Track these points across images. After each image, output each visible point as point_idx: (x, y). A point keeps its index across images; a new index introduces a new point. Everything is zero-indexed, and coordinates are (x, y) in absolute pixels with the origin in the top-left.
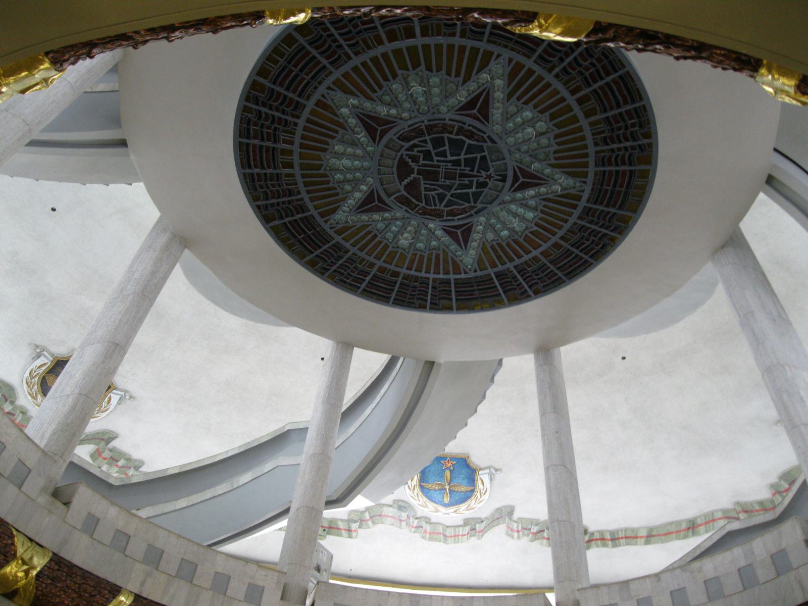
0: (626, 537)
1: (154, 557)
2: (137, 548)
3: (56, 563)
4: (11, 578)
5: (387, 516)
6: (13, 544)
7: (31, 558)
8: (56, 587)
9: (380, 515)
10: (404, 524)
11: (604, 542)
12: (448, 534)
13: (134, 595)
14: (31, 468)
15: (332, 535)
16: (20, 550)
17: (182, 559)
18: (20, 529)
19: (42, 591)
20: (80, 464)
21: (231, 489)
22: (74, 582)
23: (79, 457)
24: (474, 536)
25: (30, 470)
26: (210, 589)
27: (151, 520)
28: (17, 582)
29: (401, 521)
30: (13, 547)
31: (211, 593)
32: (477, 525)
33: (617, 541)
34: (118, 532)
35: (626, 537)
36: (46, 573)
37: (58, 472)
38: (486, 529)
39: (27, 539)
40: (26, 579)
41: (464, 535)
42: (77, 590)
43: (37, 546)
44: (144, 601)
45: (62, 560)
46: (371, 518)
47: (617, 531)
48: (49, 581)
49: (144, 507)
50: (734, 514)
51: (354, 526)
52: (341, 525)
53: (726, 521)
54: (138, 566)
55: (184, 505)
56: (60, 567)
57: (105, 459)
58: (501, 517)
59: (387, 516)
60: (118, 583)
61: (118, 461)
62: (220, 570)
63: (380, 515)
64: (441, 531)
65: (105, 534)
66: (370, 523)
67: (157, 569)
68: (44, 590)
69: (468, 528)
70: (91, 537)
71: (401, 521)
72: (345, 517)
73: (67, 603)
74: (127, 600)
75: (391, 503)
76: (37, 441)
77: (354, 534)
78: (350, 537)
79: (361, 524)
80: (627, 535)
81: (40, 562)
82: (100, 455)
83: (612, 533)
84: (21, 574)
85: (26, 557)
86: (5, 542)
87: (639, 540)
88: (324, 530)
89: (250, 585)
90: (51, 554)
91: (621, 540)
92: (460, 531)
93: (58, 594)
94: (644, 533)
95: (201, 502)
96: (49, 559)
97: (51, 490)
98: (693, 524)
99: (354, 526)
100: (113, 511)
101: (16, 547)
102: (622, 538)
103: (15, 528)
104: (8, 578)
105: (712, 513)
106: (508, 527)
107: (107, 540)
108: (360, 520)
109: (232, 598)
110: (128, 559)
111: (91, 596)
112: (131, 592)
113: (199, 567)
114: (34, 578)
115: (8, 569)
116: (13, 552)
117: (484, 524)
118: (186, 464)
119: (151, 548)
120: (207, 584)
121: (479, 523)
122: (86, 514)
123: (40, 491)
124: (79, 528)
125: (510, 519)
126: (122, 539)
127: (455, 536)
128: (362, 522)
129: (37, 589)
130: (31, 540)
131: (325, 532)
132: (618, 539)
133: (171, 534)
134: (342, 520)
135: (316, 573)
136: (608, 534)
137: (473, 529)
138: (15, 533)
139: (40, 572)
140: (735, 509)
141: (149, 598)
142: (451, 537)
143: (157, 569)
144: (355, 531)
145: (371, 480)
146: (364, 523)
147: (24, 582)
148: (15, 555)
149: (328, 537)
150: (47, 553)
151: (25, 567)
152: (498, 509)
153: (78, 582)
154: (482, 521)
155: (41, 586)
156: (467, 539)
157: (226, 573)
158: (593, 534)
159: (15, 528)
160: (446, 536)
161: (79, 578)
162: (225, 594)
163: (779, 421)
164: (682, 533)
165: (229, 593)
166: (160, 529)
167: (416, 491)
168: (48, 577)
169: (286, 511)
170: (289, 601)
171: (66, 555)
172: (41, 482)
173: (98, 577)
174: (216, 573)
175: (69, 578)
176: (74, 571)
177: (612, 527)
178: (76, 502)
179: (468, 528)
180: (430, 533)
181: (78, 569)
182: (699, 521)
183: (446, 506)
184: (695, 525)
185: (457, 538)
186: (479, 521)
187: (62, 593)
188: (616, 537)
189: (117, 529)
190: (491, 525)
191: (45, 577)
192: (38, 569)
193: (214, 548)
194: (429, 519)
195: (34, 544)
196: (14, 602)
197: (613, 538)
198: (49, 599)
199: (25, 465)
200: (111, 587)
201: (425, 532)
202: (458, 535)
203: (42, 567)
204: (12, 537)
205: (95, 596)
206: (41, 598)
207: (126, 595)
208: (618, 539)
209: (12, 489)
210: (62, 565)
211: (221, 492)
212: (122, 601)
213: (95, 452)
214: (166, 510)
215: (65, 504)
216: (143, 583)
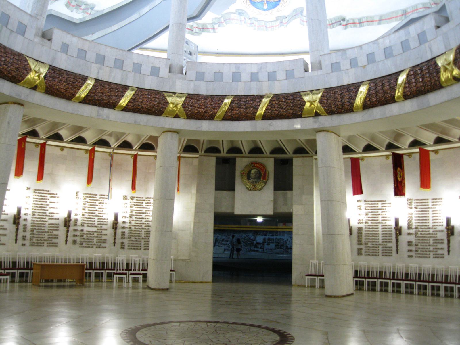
0: (367, 21)
1: (101, 59)
2: (91, 56)
3: (52, 70)
4: (32, 80)
5: (233, 19)
6: (28, 64)
7: (39, 70)
8: (55, 81)
9: (229, 19)
10: (243, 22)
11: (355, 24)
12: (268, 26)
13: (94, 79)
14: (26, 25)
15: (205, 32)
16: (33, 67)
17: (115, 59)
18: (30, 56)
19: (49, 84)
20: (56, 14)
21: (139, 16)
22: (63, 77)
23: (55, 11)
24: (282, 26)
25: (26, 26)
26: (132, 72)
27: (95, 41)
28: (36, 82)
29: (241, 21)
30: (29, 66)
31: (133, 73)
32: (284, 20)
33: (362, 24)
34: (80, 50)
35: (367, 21)
36: (48, 75)
37: (42, 24)
38: (289, 22)
39: (34, 60)
40: (39, 79)
41: (277, 26)
42: (66, 81)
43: (41, 63)
44: (100, 82)
45: (55, 68)
46: (224, 21)
47: (362, 18)
48: (51, 79)
49: (95, 32)
50: (429, 6)
51: (216, 26)
52: (209, 27)
53: (424, 9)
54: (94, 65)
55: (116, 28)
56: (54, 71)
57: (73, 6)
58: (297, 14)
59: (233, 19)
60: (86, 75)
61: (80, 6)
62: (136, 62)
63: (229, 19)
64: (264, 25)
65: (73, 51)
66: (224, 24)
67: (103, 65)
68: (50, 84)
69: (278, 22)
70: (67, 54)
71: (241, 21)
72: (211, 22)
73: (62, 88)
74: (91, 82)
75: (235, 12)
76: (26, 10)
77: (216, 31)
78: (214, 32)
79: (219, 25)
80: (368, 20)
81: (44, 71)
82: (70, 4)
83: (359, 19)
84: (36, 78)
85: (37, 69)
86: (24, 64)
87: (374, 22)
88: (200, 30)
89: (152, 67)
90: (48, 66)
91: (364, 23)
92: (275, 24)
93: (57, 84)
94: (377, 18)
95: (125, 26)
96: (48, 68)
97: (40, 34)
98: (406, 12)
99: (216, 26)
100: (75, 39)
101: (30, 65)
102: (365, 22)
103: (27, 56)
104: (30, 80)
105: (417, 6)
106: (301, 20)
107: (75, 55)
108: (219, 23)
109: (144, 75)
110: (88, 62)
111: (73, 83)
112: (93, 78)
113: (125, 61)
114: (43, 78)
115: (29, 76)
116: (29, 68)
117: (287, 20)
118: (114, 6)
119: (98, 55)
120: (131, 69)
121: (284, 19)
122: (61, 43)
123: (35, 36)
124: (59, 50)
125: (302, 15)
126: (82, 53)
127: (272, 27)
128: (220, 23)
129: (46, 83)
130: (37, 61)
131: (201, 31)
132: (363, 22)
133: (107, 47)
134: (209, 24)
135: (189, 56)
136: (357, 20)
137: (282, 22)
138: (28, 58)
139: (45, 75)
140: (430, 3)
141: (102, 80)
142: (270, 27)
143: (103, 65)
144: (217, 29)
145: (211, 6)
146: (221, 24)
147: (39, 81)
148: (31, 69)
149: (203, 33)
150: (46, 66)
151: (37, 74)
152: (295, 10)
153: (65, 77)
154: (286, 18)
155: (48, 82)
156: (279, 28)
157: (139, 62)
158: (348, 21)
159: (27, 56)
160: (266, 27)
161: (65, 75)
162: (140, 73)
163: (8, 190)
164: (399, 18)
165: (142, 72)
166: (101, 45)
167: (247, 3)
168: (50, 77)
169: (168, 27)
170: (174, 73)
171: (56, 65)
172: (34, 31)
173: (75, 73)
174: (134, 63)
175: (60, 76)
176: (62, 72)
177: (359, 16)
178: (54, 38)
179: (278, 22)
180: (258, 26)
181: (64, 71)
182: (409, 11)
183: (265, 10)
184: (407, 13)
185: (273, 28)
186: (284, 17)
187: (59, 83)
188: (362, 21)
189: (79, 49)
190: (291, 19)
191: (48, 77)
192: (44, 74)
193: (131, 51)
194: (257, 19)
195: (39, 62)
196: (37, 91)
197: (360, 22)
198: (53, 87)
199: (23, 24)
200: (82, 77)
201: (255, 26)
202: (274, 26)
203: (45, 73)
204: (26, 61)
205: (75, 82)
206: (49, 87)
207: (91, 80)
208: (363, 22)
209: (20, 37)
210: (56, 70)
211: (134, 19)
212: (89, 83)
213: (67, 3)
214: (107, 33)
215: (49, 40)
216: (98, 73)
